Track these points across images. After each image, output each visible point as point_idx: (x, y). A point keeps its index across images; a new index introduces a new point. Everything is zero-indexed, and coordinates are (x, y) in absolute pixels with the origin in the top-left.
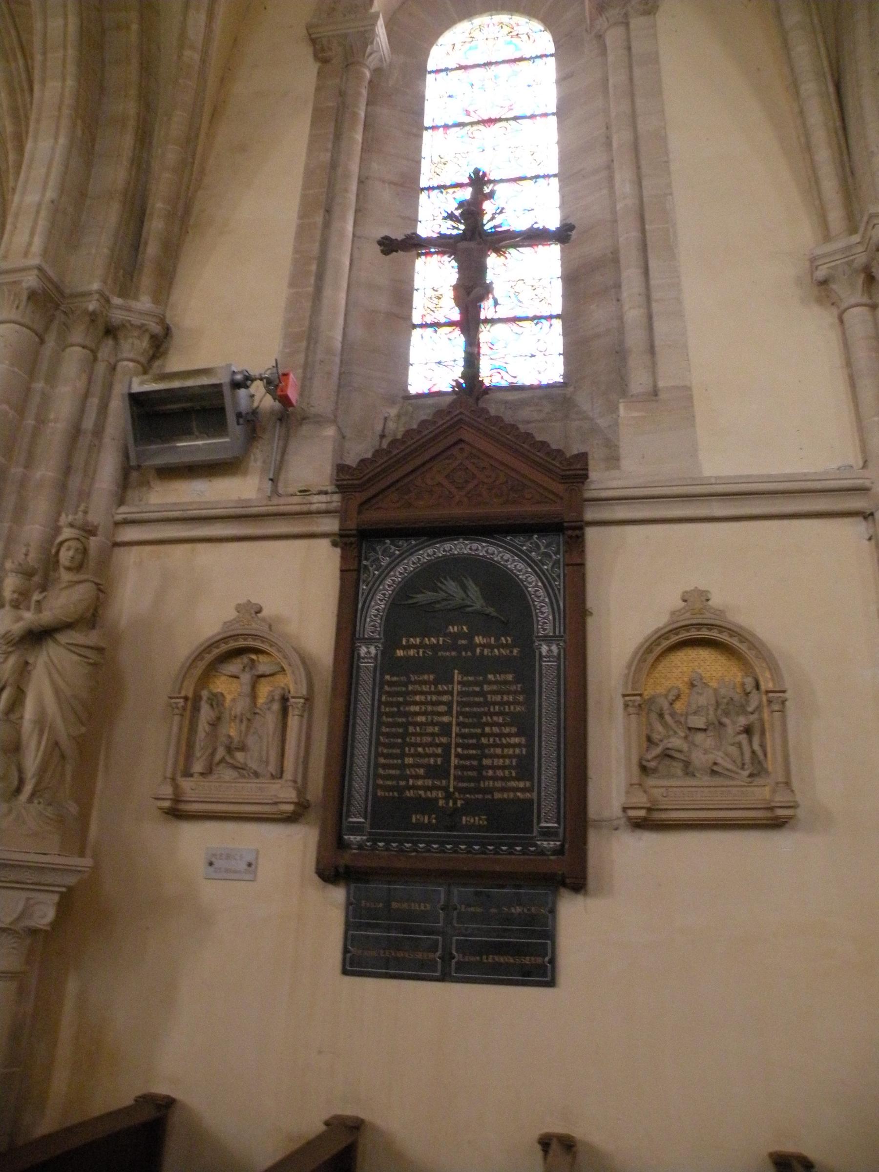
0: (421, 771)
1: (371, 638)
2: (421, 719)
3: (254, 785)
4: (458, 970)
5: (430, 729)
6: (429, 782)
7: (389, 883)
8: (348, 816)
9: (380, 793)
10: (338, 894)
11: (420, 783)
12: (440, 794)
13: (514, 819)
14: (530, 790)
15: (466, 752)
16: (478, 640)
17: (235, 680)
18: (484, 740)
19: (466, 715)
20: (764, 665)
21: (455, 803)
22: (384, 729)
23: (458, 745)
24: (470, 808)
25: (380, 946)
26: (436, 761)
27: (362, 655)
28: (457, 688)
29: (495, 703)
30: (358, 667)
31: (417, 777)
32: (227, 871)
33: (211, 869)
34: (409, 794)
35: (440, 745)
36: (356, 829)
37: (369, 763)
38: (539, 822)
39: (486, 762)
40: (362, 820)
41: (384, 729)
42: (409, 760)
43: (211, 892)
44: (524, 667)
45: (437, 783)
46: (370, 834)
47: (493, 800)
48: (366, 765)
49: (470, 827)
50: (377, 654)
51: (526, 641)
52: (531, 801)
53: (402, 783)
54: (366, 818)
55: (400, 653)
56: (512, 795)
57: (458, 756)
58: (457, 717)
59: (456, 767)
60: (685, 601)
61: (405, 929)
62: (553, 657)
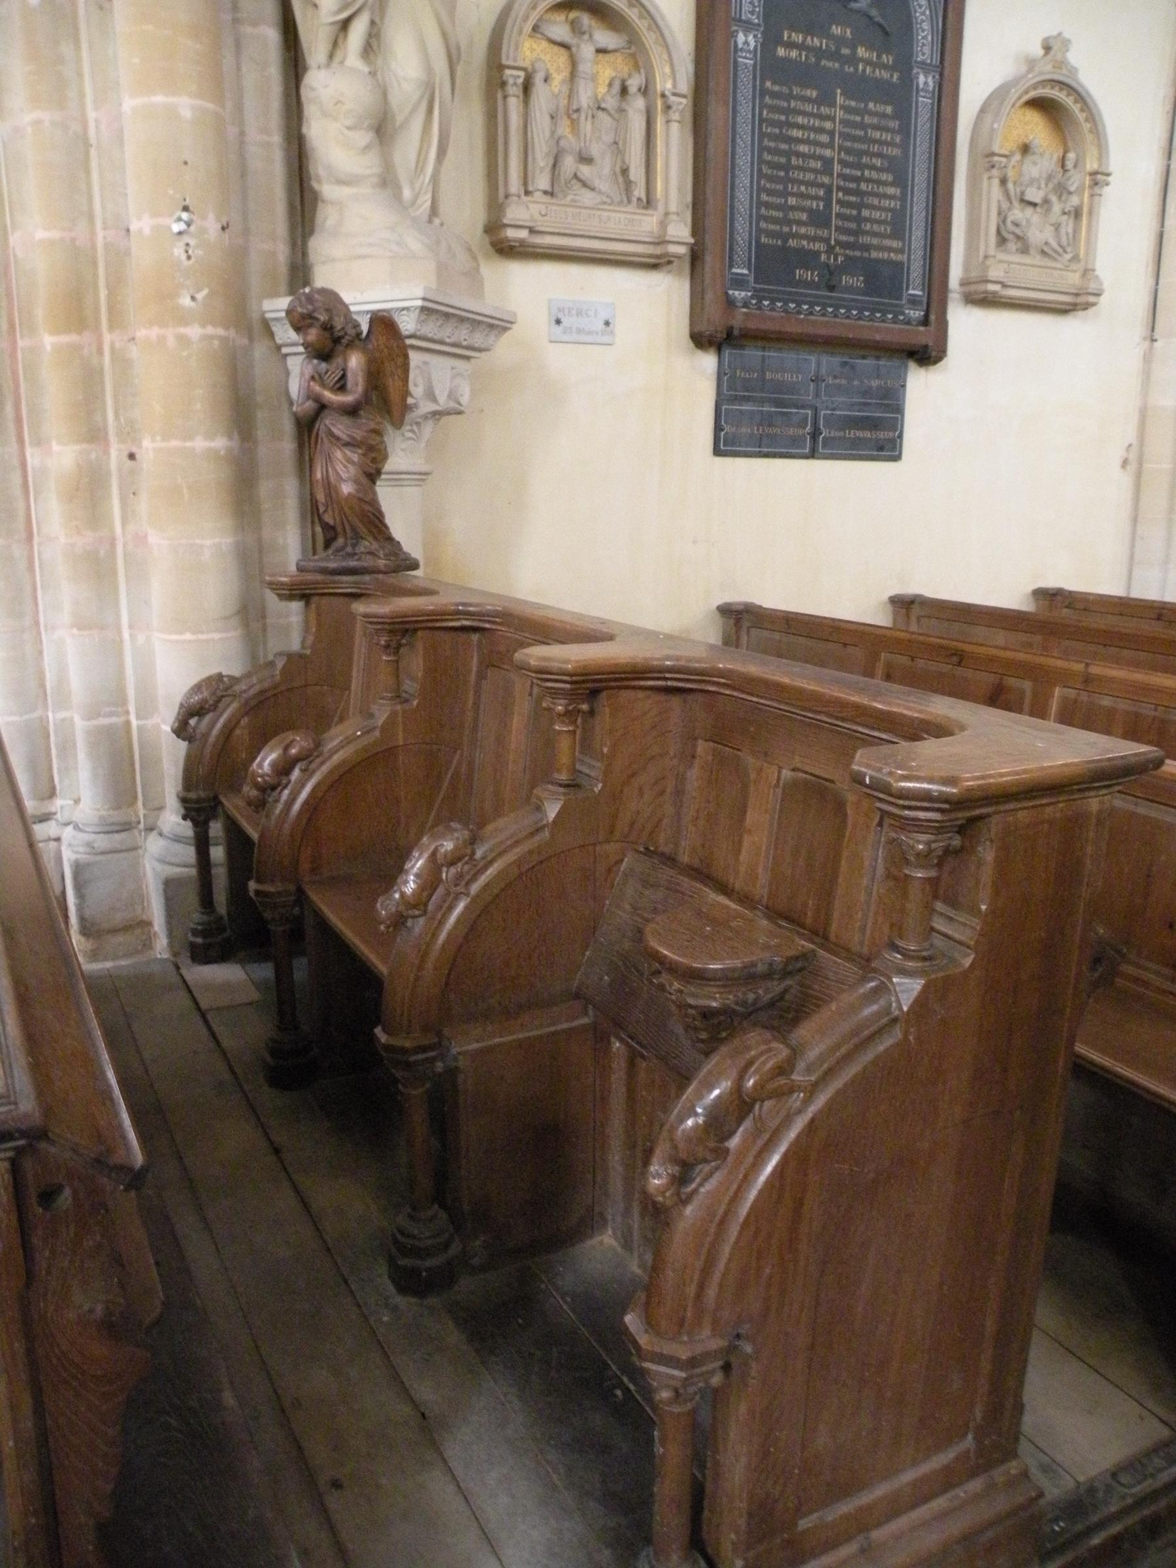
0: (804, 217)
1: (748, 22)
2: (804, 148)
3: (623, 216)
4: (824, 446)
5: (813, 164)
6: (811, 231)
7: (764, 349)
8: (731, 267)
9: (763, 240)
10: (708, 362)
11: (803, 230)
12: (821, 246)
13: (883, 282)
14: (902, 251)
15: (846, 198)
16: (861, 52)
17: (562, 50)
18: (863, 186)
19: (849, 151)
20: (665, 56)
21: (836, 259)
22: (767, 157)
23: (839, 188)
24: (850, 266)
25: (752, 424)
26: (818, 206)
27: (740, 46)
28: (839, 114)
29: (875, 141)
30: (735, 62)
31: (799, 223)
32: (579, 331)
33: (558, 330)
34: (792, 243)
35: (822, 185)
36: (739, 282)
37: (751, 197)
38: (907, 288)
39: (865, 213)
40: (745, 271)
41: (767, 157)
42: (792, 201)
43: (561, 360)
44: (900, 96)
45: (819, 232)
46: (755, 290)
47: (870, 260)
48: (748, 202)
49: (849, 289)
50: (756, 47)
51: (905, 65)
52: (901, 264)
53: (786, 229)
54: (750, 270)
55: (781, 52)
56: (886, 255)
57: (839, 201)
58: (839, 153)
59: (838, 215)
60: (1047, 48)
61: (779, 403)
62: (749, 51)
